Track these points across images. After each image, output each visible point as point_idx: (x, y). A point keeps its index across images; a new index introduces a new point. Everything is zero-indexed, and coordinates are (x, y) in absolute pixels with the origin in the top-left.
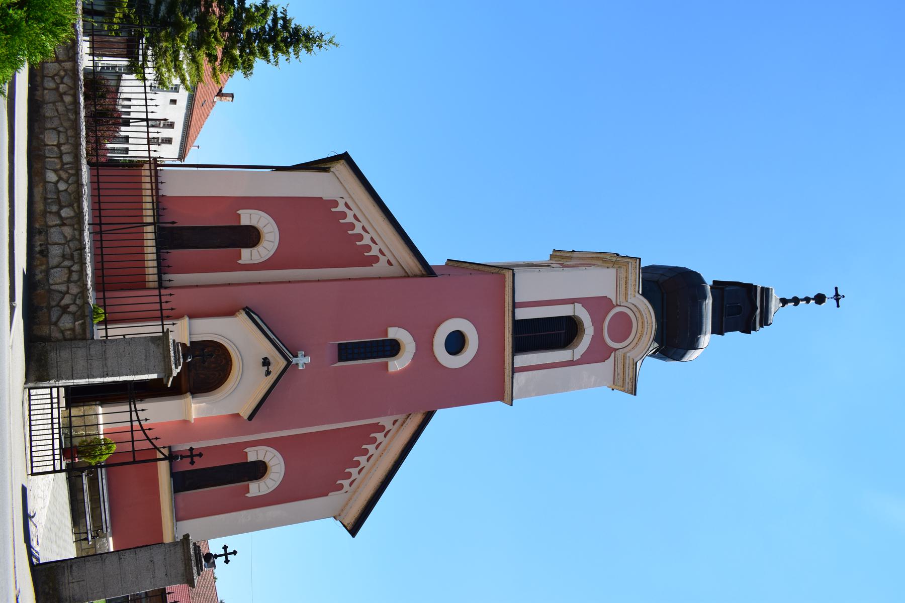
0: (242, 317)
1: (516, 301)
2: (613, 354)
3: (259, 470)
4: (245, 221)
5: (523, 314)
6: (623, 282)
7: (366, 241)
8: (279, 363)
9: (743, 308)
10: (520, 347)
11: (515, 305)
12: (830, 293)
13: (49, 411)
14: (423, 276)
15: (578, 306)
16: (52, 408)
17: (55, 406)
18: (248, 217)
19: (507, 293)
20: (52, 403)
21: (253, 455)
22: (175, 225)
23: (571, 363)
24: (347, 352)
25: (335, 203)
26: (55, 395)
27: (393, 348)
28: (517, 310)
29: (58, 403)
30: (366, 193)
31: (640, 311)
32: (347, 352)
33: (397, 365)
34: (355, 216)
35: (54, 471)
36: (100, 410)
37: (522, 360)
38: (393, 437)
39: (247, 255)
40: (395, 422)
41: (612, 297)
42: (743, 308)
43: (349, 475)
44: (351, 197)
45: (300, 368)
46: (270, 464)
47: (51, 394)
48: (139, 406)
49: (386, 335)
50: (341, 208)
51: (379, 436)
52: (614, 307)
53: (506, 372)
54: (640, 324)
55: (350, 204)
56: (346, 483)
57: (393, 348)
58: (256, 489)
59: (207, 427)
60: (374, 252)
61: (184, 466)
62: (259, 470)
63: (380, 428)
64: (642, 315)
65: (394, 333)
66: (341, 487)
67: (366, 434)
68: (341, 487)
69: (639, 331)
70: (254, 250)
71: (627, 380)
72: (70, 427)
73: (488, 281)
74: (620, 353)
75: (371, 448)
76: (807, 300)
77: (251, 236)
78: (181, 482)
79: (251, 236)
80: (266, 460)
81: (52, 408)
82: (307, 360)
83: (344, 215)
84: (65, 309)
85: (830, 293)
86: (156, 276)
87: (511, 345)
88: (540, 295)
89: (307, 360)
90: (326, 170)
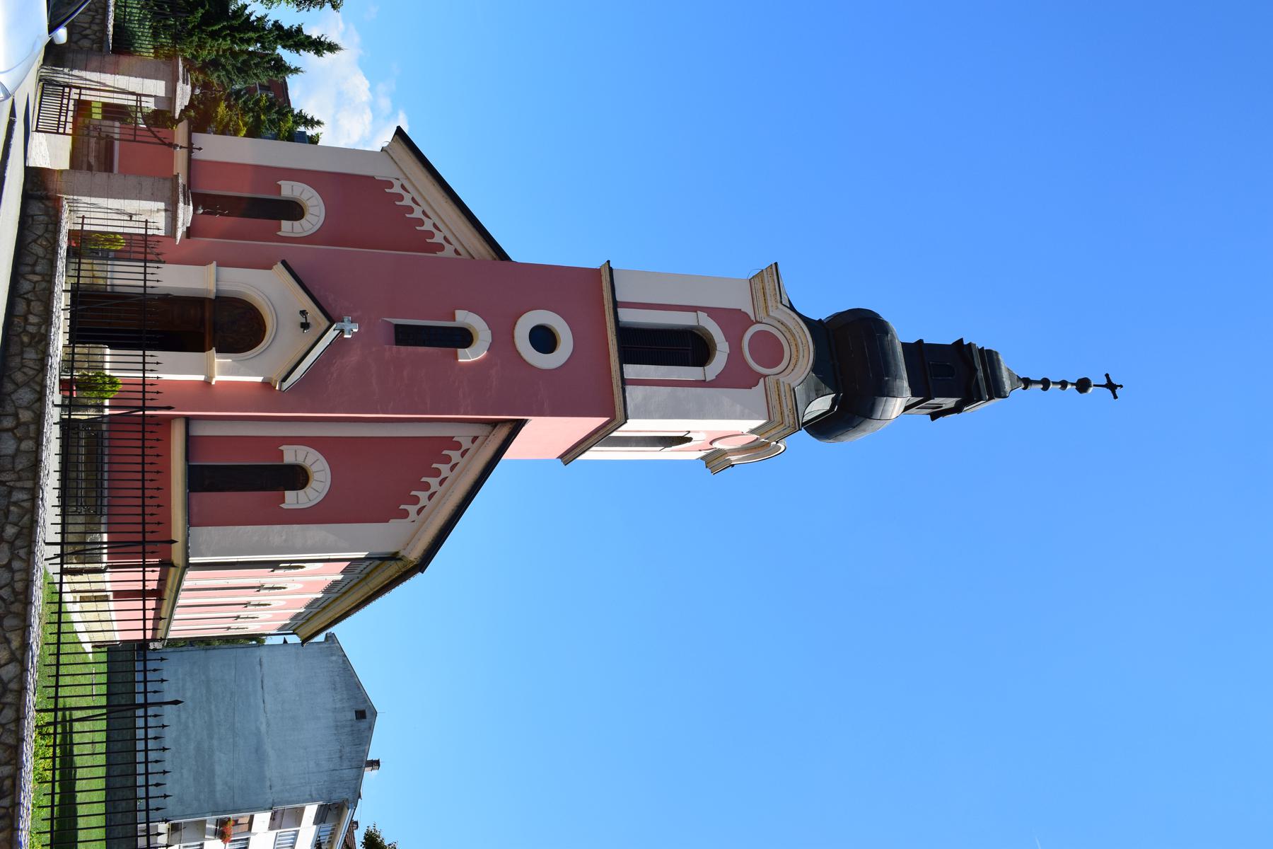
0: (279, 268)
1: (619, 299)
2: (762, 380)
3: (297, 477)
5: (627, 316)
6: (760, 294)
9: (957, 375)
10: (628, 356)
11: (616, 305)
12: (1097, 378)
15: (702, 315)
18: (289, 190)
19: (604, 283)
21: (292, 455)
24: (406, 336)
25: (391, 185)
28: (619, 310)
30: (430, 177)
31: (790, 330)
32: (406, 336)
33: (467, 356)
34: (413, 199)
36: (108, 351)
37: (632, 371)
38: (471, 459)
39: (287, 227)
40: (475, 439)
41: (747, 308)
42: (957, 375)
43: (416, 500)
44: (408, 178)
46: (313, 484)
48: (147, 353)
49: (453, 319)
50: (397, 189)
51: (455, 455)
52: (753, 323)
53: (614, 381)
54: (793, 348)
55: (407, 186)
56: (412, 509)
57: (464, 338)
58: (293, 500)
59: (236, 396)
60: (438, 238)
61: (207, 459)
62: (297, 477)
63: (457, 446)
64: (793, 335)
65: (464, 318)
67: (438, 449)
68: (405, 514)
69: (794, 356)
70: (296, 223)
71: (786, 412)
72: (73, 361)
73: (586, 289)
74: (771, 380)
75: (444, 469)
76: (1064, 384)
77: (294, 210)
78: (199, 479)
79: (294, 210)
83: (401, 198)
84: (86, 37)
85: (1097, 378)
87: (615, 342)
88: (651, 295)
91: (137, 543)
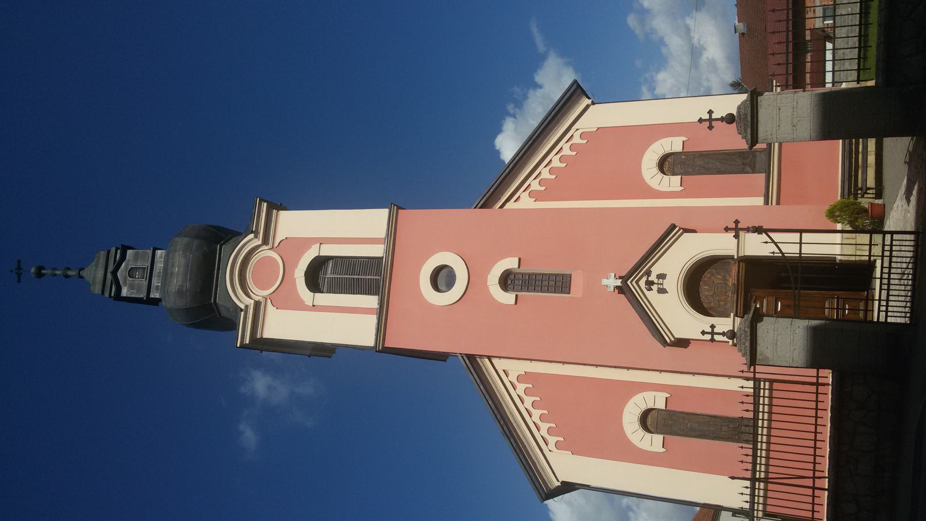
3: (666, 164)
4: (658, 438)
7: (529, 400)
8: (638, 285)
13: (891, 298)
14: (481, 356)
16: (891, 245)
17: (887, 248)
18: (654, 443)
20: (887, 306)
21: (673, 183)
22: (741, 445)
23: (322, 241)
25: (557, 445)
26: (883, 314)
27: (507, 281)
29: (880, 305)
35: (892, 233)
39: (658, 401)
45: (613, 275)
47: (887, 316)
50: (552, 440)
57: (507, 281)
58: (675, 144)
60: (521, 387)
62: (666, 164)
65: (508, 298)
66: (582, 136)
77: (647, 420)
79: (647, 420)
80: (660, 175)
81: (891, 245)
82: (605, 282)
86: (752, 390)
89: (605, 282)
90: (563, 483)
91: (811, 384)
